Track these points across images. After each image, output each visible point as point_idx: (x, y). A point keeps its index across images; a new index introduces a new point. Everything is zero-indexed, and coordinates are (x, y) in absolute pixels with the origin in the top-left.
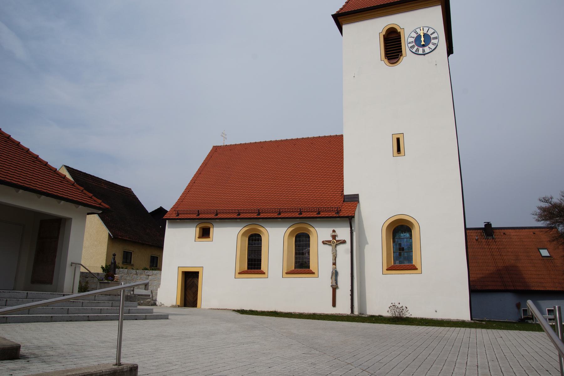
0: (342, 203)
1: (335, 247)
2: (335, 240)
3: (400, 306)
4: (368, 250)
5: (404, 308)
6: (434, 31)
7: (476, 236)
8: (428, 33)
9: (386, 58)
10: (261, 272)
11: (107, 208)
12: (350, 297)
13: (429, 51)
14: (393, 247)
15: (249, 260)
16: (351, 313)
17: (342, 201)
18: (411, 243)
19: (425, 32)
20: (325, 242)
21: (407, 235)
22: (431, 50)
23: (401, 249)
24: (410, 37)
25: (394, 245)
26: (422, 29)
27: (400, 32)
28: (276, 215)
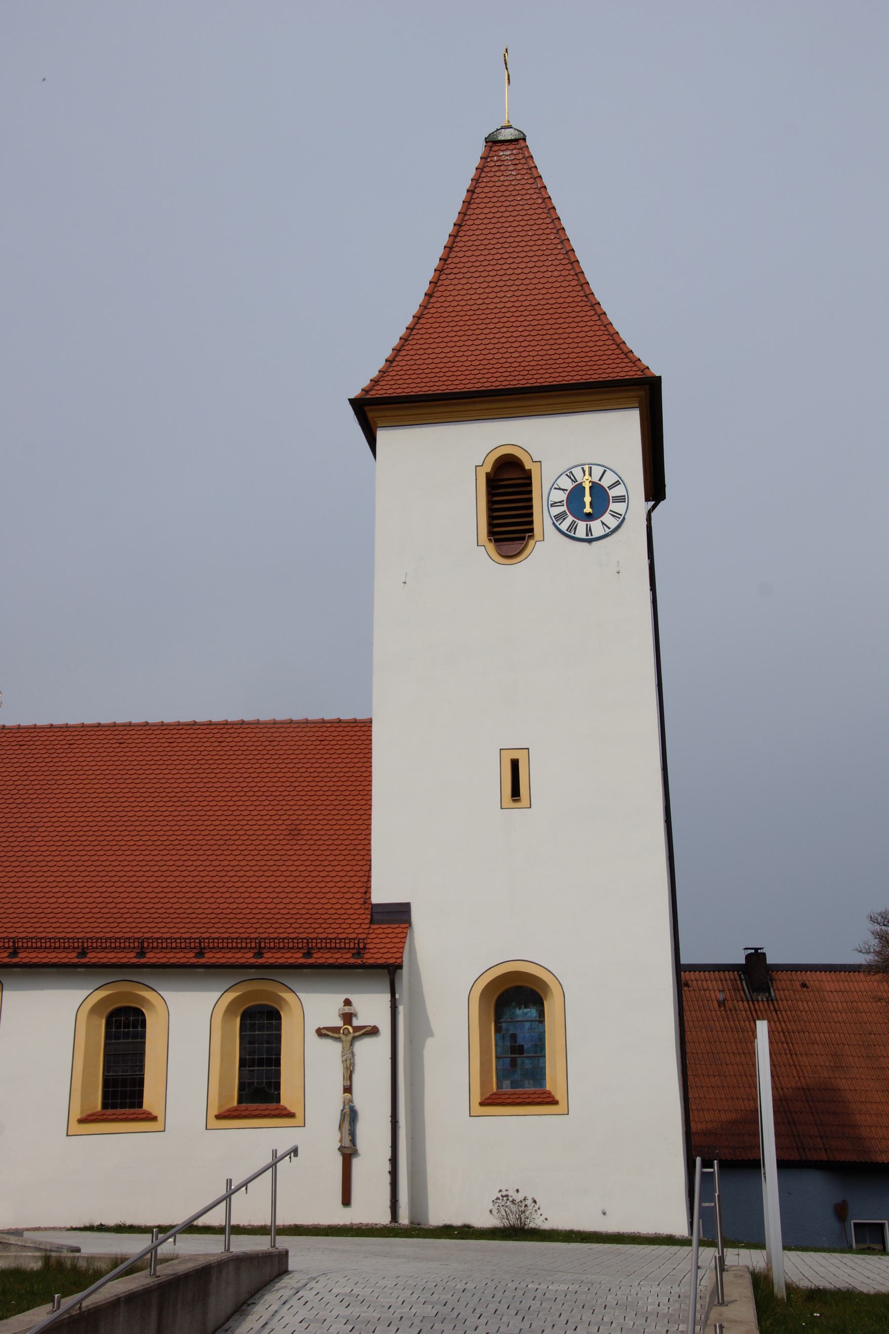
0: (367, 926)
1: (351, 1045)
2: (350, 1024)
3: (519, 1197)
4: (431, 1050)
5: (529, 1202)
6: (618, 479)
7: (720, 991)
8: (603, 483)
9: (490, 540)
10: (144, 1116)
12: (387, 1178)
13: (603, 533)
14: (496, 1045)
15: (107, 1082)
16: (391, 1222)
17: (368, 921)
18: (541, 1032)
19: (595, 479)
21: (533, 1012)
22: (608, 531)
23: (517, 1050)
24: (555, 488)
25: (498, 1038)
26: (586, 468)
27: (530, 470)
28: (189, 957)
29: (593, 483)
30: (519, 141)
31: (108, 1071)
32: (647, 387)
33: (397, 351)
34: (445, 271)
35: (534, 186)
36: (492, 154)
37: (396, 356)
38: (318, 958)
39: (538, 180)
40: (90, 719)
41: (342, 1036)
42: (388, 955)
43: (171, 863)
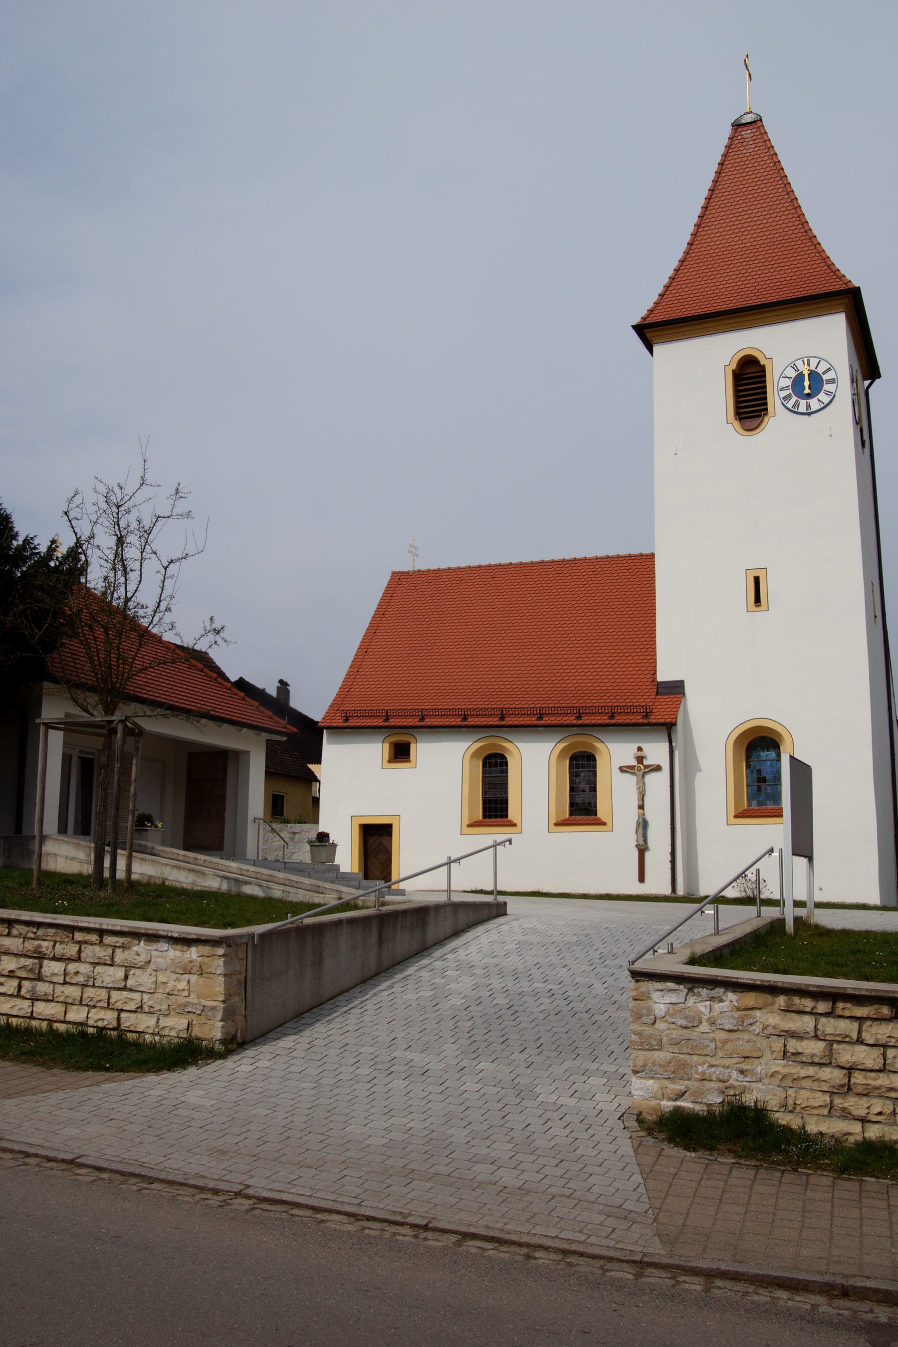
2: (642, 764)
4: (701, 782)
9: (736, 419)
11: (296, 733)
14: (747, 777)
15: (485, 802)
17: (654, 693)
19: (813, 368)
20: (625, 769)
21: (772, 754)
22: (822, 405)
23: (762, 780)
28: (533, 720)
29: (811, 371)
30: (757, 122)
31: (486, 795)
32: (850, 295)
33: (667, 287)
34: (702, 226)
35: (768, 154)
36: (737, 134)
37: (666, 291)
38: (619, 719)
39: (771, 149)
40: (474, 563)
41: (636, 772)
42: (667, 717)
43: (524, 657)
